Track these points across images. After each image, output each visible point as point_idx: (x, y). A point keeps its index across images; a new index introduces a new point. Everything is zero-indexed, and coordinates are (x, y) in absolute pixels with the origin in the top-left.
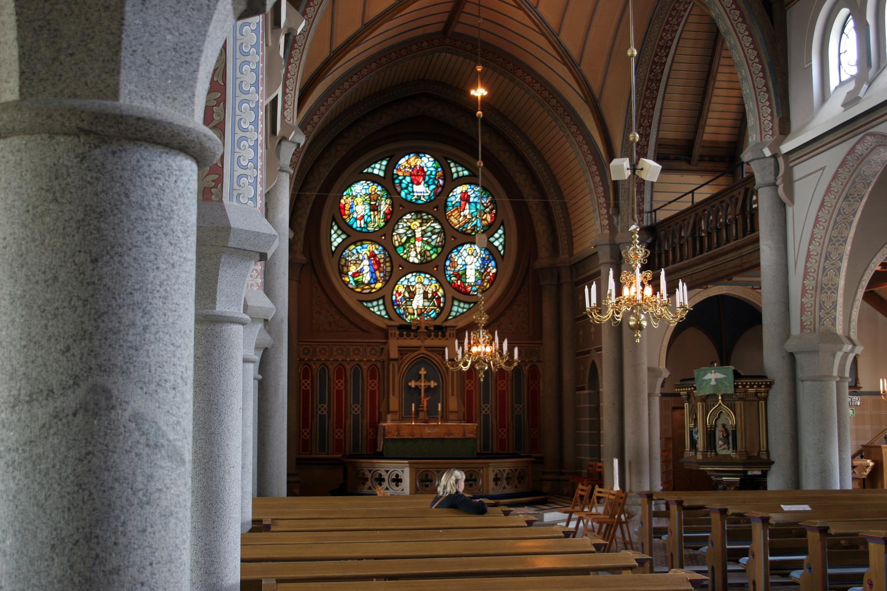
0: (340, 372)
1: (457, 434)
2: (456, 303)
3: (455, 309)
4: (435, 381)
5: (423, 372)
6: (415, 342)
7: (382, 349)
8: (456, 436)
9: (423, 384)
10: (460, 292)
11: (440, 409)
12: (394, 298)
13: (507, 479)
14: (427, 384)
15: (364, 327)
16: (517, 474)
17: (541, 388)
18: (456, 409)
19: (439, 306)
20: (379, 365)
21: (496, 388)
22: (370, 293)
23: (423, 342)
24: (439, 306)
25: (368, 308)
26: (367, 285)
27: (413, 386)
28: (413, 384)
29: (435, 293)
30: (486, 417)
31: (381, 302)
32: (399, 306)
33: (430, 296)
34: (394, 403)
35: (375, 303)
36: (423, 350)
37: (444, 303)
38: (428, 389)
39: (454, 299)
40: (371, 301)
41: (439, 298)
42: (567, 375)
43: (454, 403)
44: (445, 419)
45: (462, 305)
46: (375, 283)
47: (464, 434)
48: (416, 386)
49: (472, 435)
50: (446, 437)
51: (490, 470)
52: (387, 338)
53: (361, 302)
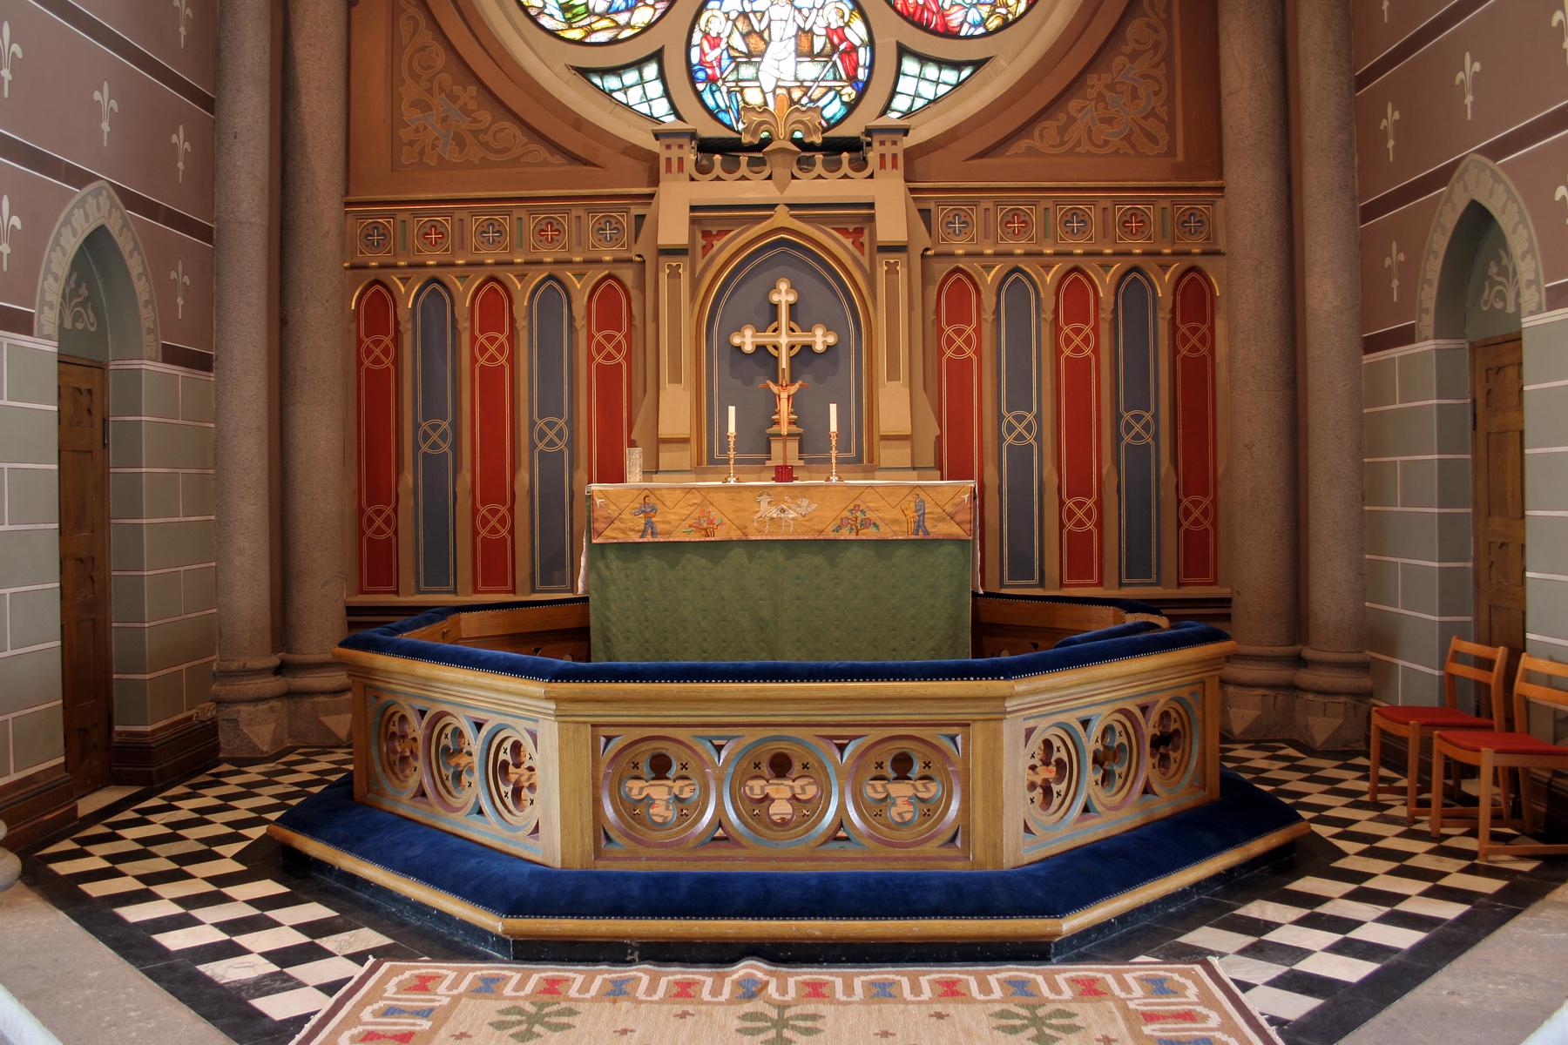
0: (494, 303)
1: (892, 522)
2: (910, 66)
3: (905, 85)
4: (829, 329)
5: (783, 296)
6: (749, 189)
7: (640, 218)
8: (887, 532)
9: (784, 340)
10: (925, 28)
11: (834, 427)
12: (695, 56)
13: (1098, 760)
14: (801, 338)
15: (573, 147)
16: (1150, 728)
17: (1221, 349)
18: (906, 428)
19: (852, 79)
20: (627, 275)
21: (1058, 352)
22: (614, 41)
23: (782, 188)
24: (852, 79)
25: (609, 94)
26: (602, 16)
27: (749, 348)
28: (747, 340)
29: (836, 34)
30: (1021, 457)
31: (651, 70)
32: (711, 80)
33: (819, 44)
34: (675, 409)
35: (631, 77)
36: (782, 218)
37: (871, 67)
38: (805, 353)
39: (903, 51)
40: (616, 71)
41: (853, 49)
42: (1326, 293)
43: (895, 407)
44: (861, 459)
45: (931, 71)
46: (630, 9)
47: (919, 524)
48: (761, 348)
49: (955, 530)
50: (846, 534)
51: (1011, 730)
52: (655, 181)
53: (585, 72)
